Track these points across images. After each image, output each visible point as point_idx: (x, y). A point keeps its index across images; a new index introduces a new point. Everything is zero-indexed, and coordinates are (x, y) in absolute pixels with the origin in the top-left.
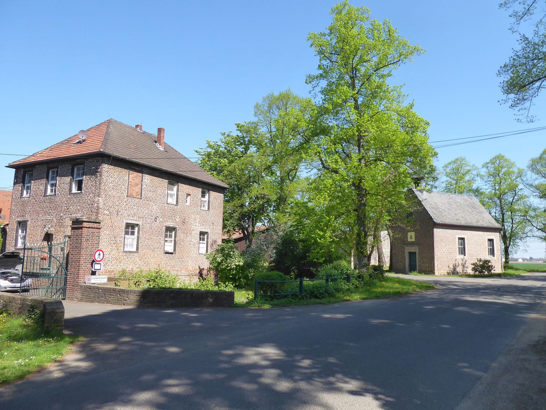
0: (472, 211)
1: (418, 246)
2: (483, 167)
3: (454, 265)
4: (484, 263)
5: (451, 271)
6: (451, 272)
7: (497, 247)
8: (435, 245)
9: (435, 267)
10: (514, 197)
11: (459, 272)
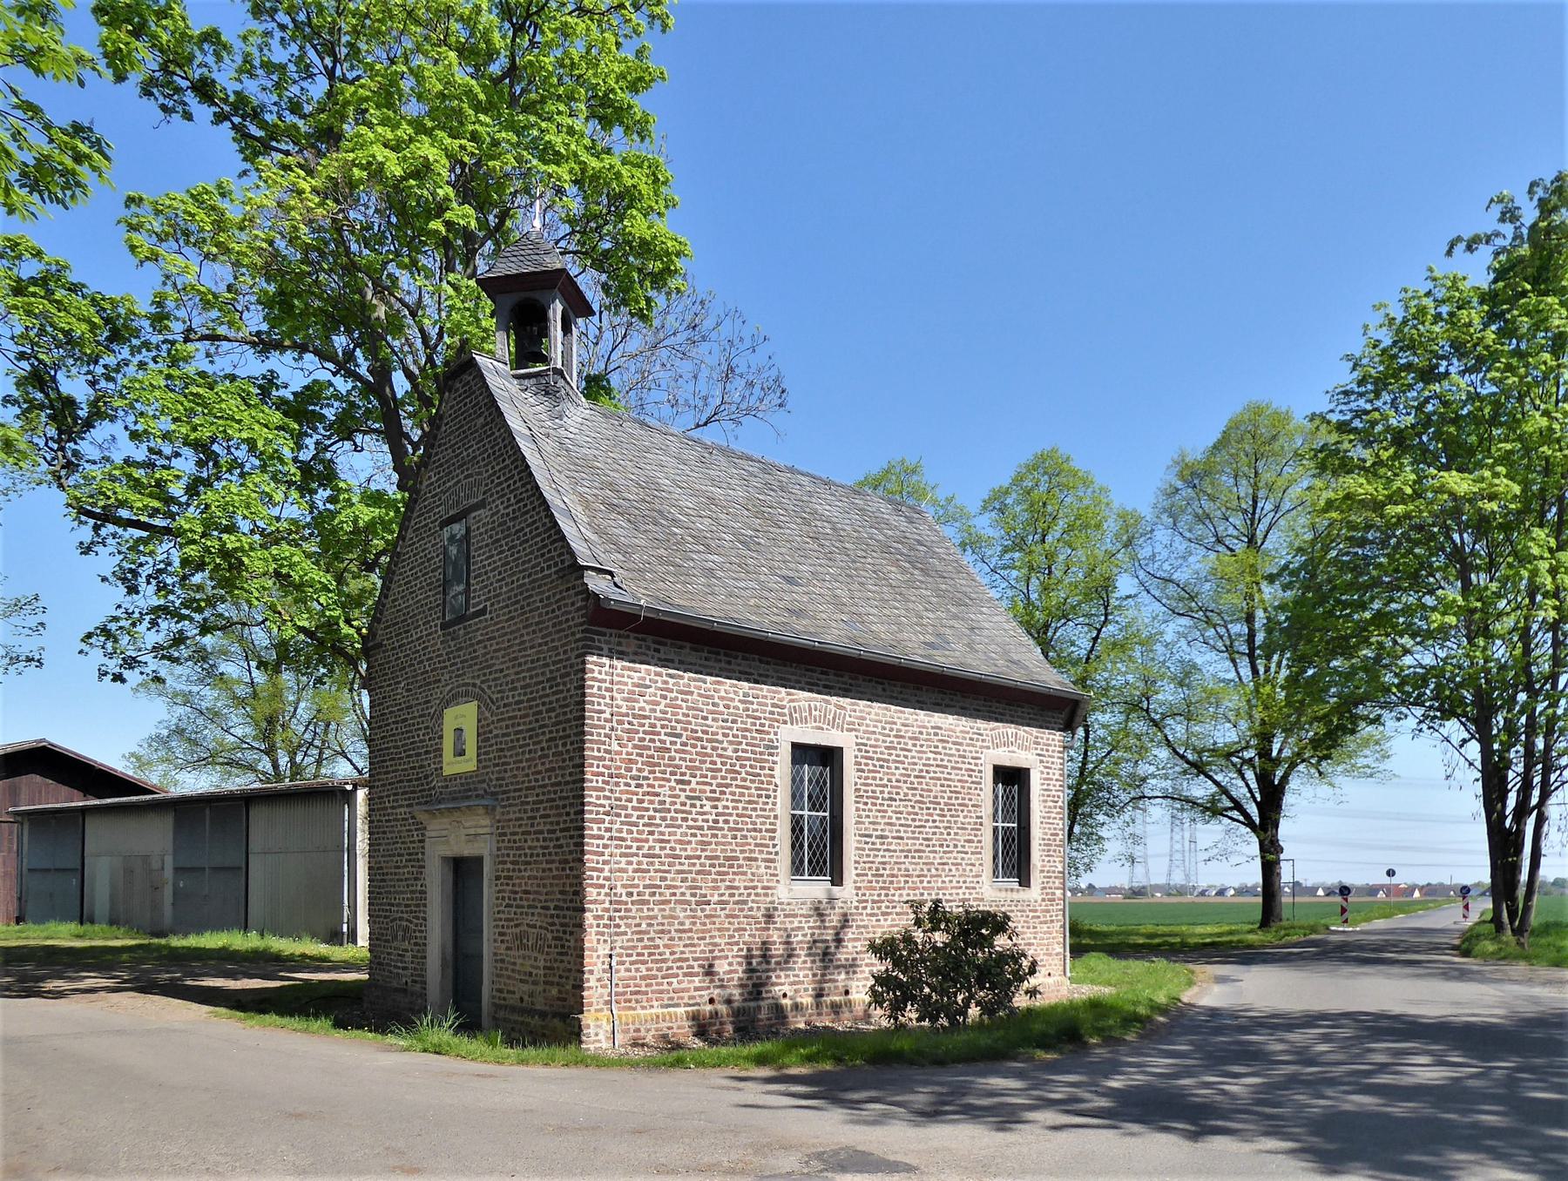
0: (910, 584)
1: (489, 810)
2: (984, 508)
3: (749, 957)
4: (965, 933)
5: (729, 1001)
6: (722, 1008)
7: (1045, 819)
8: (591, 797)
9: (591, 981)
10: (1099, 631)
11: (786, 1002)
